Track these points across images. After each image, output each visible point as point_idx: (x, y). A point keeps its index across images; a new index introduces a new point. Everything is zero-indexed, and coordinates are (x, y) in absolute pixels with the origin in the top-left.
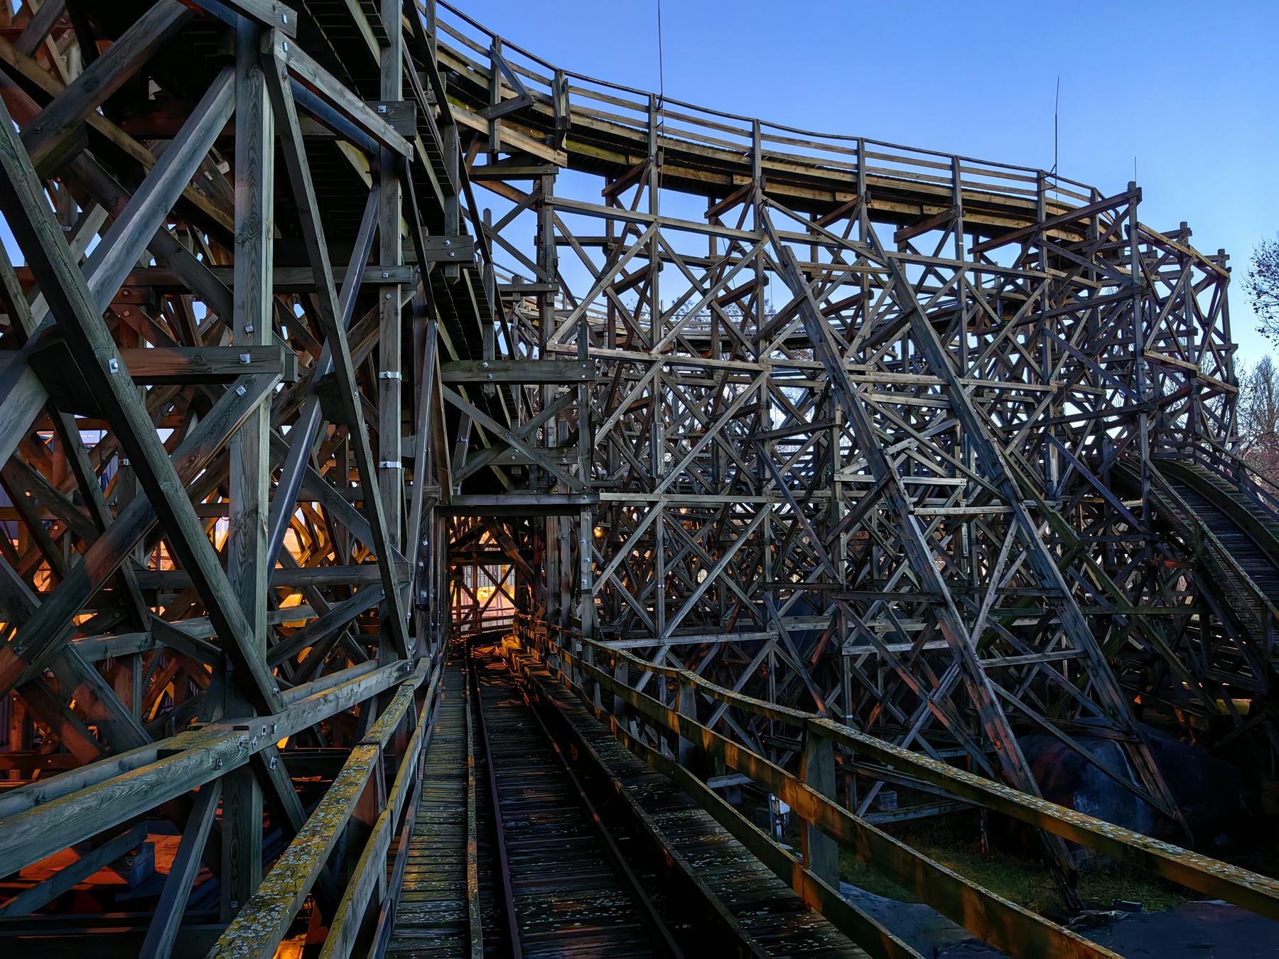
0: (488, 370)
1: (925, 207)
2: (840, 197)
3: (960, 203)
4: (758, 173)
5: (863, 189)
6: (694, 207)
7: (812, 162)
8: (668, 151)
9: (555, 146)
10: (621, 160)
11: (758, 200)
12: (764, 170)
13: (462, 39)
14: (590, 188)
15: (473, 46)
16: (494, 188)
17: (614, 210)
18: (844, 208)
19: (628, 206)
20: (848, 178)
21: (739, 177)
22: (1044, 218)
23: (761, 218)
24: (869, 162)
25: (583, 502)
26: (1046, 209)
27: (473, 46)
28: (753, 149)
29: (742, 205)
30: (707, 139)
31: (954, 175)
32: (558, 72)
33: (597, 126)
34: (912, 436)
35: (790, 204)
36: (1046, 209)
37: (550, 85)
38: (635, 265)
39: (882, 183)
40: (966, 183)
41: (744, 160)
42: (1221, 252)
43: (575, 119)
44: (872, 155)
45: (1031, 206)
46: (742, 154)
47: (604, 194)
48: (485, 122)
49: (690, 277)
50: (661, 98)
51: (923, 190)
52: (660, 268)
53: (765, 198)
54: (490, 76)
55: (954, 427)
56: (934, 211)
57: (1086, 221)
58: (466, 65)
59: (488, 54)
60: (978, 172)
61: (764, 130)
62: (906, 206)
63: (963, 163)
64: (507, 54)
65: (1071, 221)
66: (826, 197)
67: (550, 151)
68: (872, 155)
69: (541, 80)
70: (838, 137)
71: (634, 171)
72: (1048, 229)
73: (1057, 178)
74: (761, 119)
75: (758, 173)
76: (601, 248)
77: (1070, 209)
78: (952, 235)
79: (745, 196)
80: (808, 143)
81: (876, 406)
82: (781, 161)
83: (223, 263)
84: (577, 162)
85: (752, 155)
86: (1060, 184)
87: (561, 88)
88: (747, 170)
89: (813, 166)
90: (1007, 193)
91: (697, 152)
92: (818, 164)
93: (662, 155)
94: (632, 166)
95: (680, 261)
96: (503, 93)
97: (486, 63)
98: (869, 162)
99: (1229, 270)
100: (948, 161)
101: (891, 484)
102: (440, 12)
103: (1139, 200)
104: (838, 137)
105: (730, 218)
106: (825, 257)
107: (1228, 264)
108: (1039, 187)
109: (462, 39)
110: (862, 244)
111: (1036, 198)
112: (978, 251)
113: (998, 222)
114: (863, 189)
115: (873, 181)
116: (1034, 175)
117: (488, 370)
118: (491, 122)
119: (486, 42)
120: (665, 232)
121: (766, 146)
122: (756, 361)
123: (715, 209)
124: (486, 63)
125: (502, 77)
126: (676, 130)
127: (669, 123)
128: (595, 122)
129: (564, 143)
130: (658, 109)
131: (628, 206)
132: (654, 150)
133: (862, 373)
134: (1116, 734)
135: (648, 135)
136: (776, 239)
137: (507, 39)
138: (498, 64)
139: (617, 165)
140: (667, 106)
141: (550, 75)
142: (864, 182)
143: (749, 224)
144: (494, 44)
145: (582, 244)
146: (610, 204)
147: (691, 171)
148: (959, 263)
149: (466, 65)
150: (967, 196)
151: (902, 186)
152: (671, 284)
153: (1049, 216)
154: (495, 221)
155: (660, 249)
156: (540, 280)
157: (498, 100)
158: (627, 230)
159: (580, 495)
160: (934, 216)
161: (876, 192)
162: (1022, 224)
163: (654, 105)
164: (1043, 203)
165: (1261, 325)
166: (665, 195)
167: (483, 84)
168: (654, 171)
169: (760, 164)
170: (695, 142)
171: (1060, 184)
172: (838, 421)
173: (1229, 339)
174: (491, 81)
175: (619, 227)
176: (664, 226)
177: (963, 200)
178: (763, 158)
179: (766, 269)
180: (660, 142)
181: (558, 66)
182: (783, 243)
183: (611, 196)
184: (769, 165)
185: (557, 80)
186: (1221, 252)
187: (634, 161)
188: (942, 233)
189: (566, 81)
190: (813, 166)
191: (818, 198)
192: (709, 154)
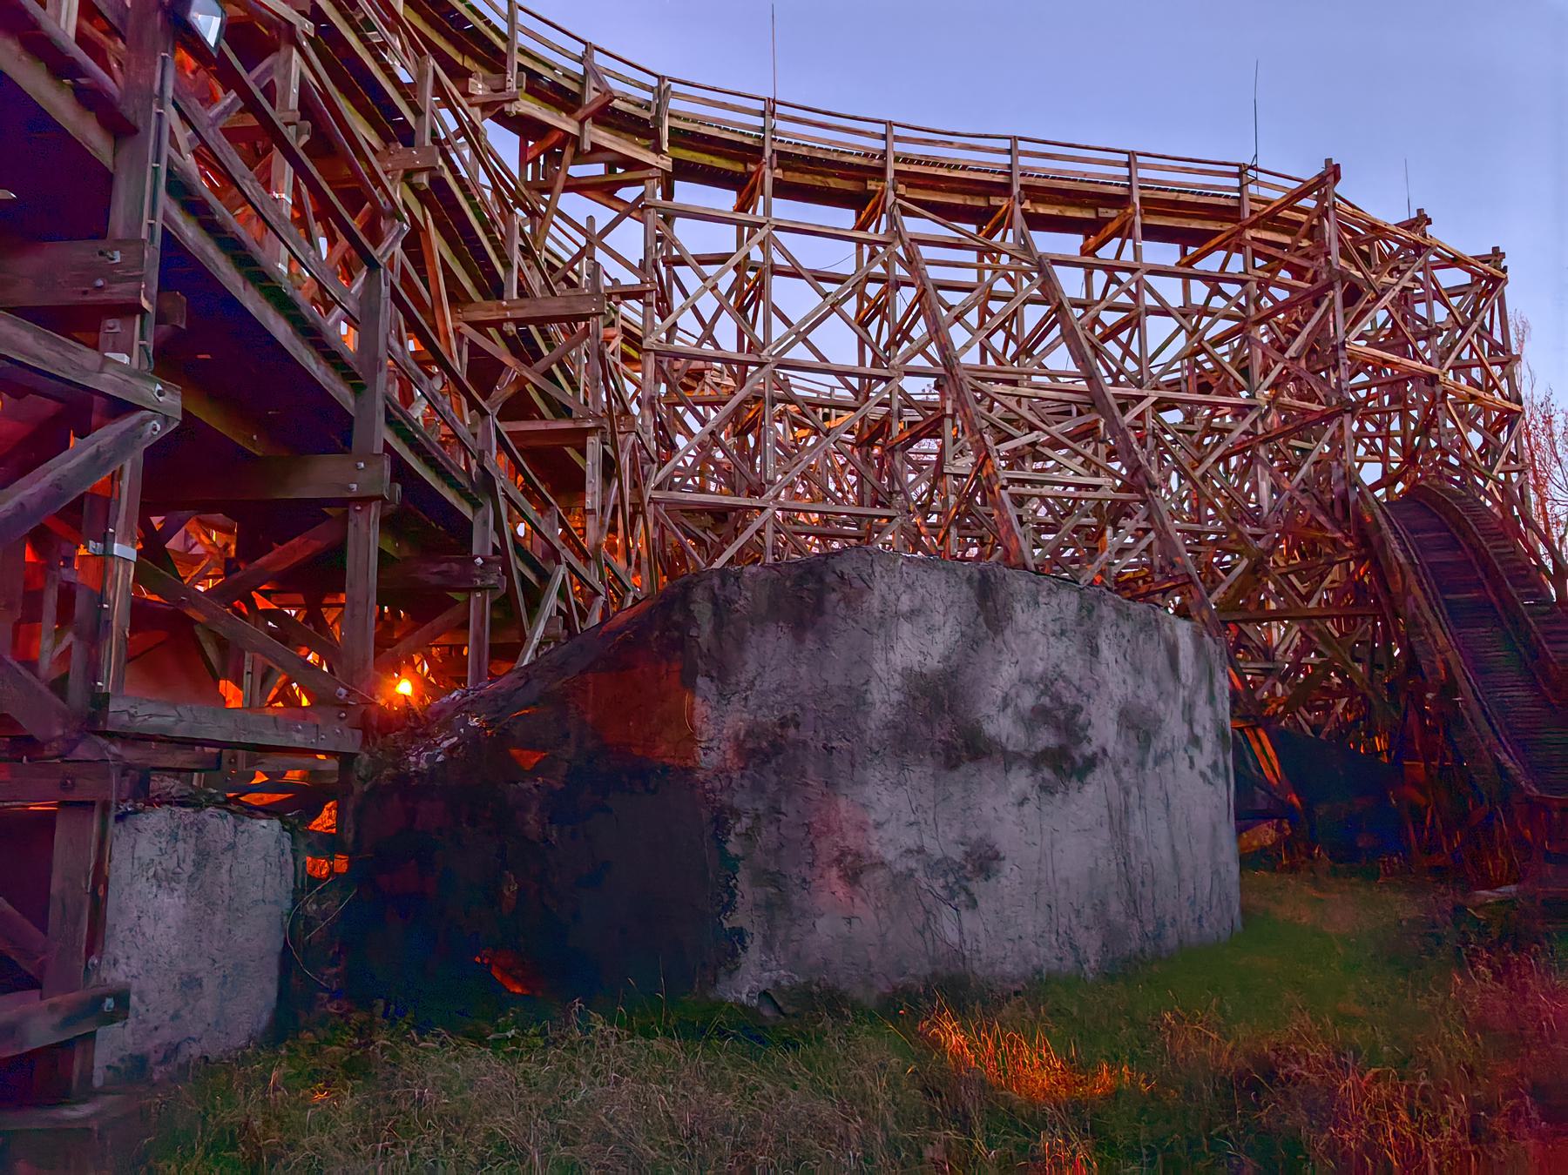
0: (506, 309)
1: (1100, 210)
3: (1136, 200)
4: (890, 175)
8: (782, 155)
10: (739, 168)
12: (897, 172)
13: (551, 46)
15: (563, 52)
16: (594, 196)
20: (1000, 179)
21: (873, 183)
22: (1247, 215)
24: (1023, 161)
26: (1248, 206)
27: (563, 52)
30: (830, 143)
32: (661, 78)
33: (704, 130)
34: (1040, 429)
39: (1041, 183)
41: (876, 162)
42: (1495, 249)
45: (1231, 203)
46: (874, 156)
48: (576, 124)
49: (819, 290)
50: (774, 101)
54: (582, 81)
55: (1097, 421)
58: (553, 69)
59: (580, 60)
60: (1161, 168)
62: (1077, 209)
63: (1140, 159)
64: (599, 60)
66: (980, 202)
67: (653, 155)
69: (643, 87)
70: (986, 136)
73: (1258, 170)
74: (894, 120)
77: (1268, 202)
80: (951, 143)
81: (996, 396)
85: (884, 154)
86: (1262, 177)
87: (662, 94)
88: (880, 173)
90: (1202, 191)
91: (819, 156)
96: (591, 96)
97: (579, 69)
98: (1023, 161)
99: (1505, 270)
100: (1125, 158)
102: (522, 18)
103: (1337, 178)
104: (986, 136)
108: (1241, 182)
109: (551, 46)
110: (1016, 247)
113: (1195, 225)
114: (1016, 190)
116: (1236, 170)
117: (506, 309)
118: (582, 123)
119: (579, 49)
121: (899, 147)
124: (579, 69)
125: (592, 83)
126: (795, 134)
127: (781, 126)
128: (702, 127)
130: (773, 114)
132: (768, 153)
137: (600, 46)
138: (591, 71)
139: (735, 173)
140: (779, 109)
141: (653, 82)
147: (819, 178)
148: (1137, 265)
149: (553, 69)
150: (1147, 194)
151: (1065, 185)
163: (770, 109)
167: (574, 88)
170: (817, 145)
171: (1262, 177)
172: (949, 411)
174: (582, 85)
176: (778, 228)
177: (1142, 199)
178: (896, 160)
180: (776, 146)
181: (660, 73)
185: (659, 87)
186: (1495, 249)
188: (1119, 240)
191: (969, 202)
192: (835, 157)
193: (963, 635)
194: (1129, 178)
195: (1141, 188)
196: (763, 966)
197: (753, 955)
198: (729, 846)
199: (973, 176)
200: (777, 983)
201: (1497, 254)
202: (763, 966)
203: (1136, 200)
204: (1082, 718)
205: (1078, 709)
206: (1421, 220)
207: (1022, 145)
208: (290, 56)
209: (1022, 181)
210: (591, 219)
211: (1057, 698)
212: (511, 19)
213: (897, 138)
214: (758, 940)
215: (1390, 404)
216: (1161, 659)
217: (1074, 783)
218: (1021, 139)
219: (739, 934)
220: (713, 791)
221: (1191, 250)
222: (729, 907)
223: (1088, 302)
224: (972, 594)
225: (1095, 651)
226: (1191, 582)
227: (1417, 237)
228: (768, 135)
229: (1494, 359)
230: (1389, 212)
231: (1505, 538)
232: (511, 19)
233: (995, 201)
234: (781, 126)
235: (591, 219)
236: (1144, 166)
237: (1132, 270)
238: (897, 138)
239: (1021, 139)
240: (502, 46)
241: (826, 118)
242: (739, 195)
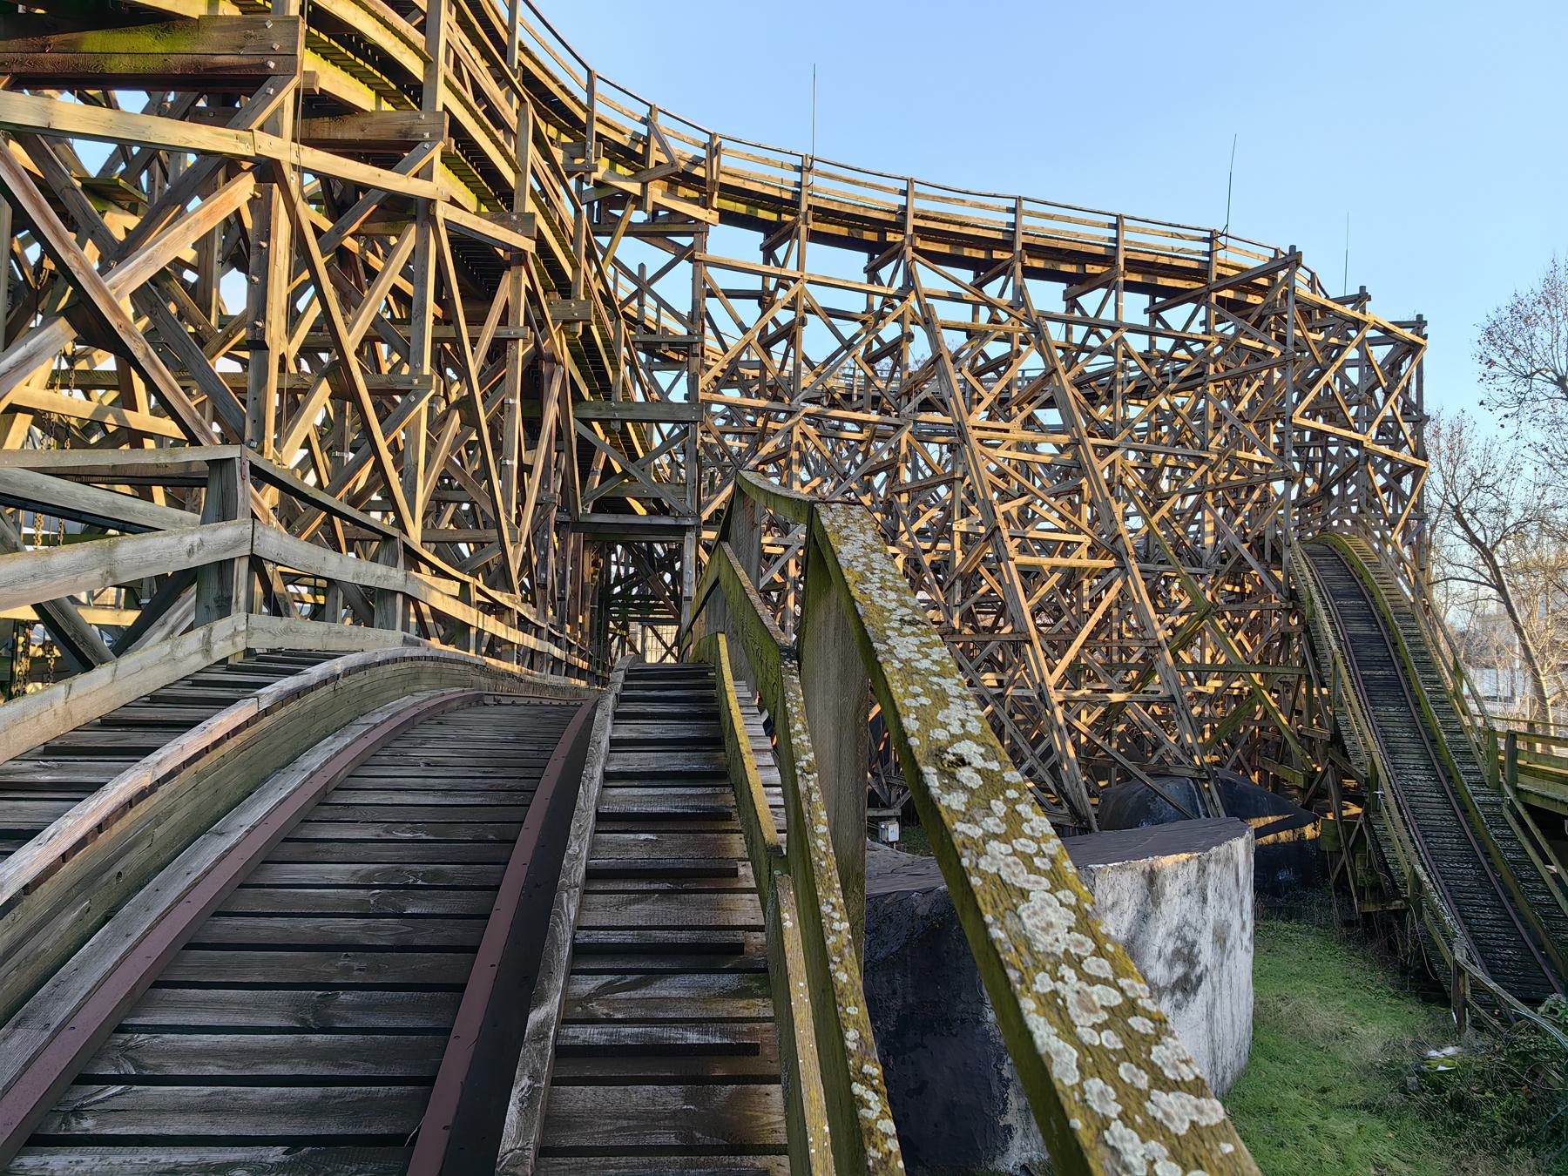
0: (615, 410)
2: (997, 255)
3: (1121, 262)
5: (1019, 247)
6: (853, 263)
7: (966, 221)
8: (816, 209)
9: (705, 203)
10: (773, 217)
11: (908, 258)
12: (916, 228)
14: (742, 245)
17: (875, 288)
18: (1001, 266)
19: (886, 281)
22: (1214, 279)
23: (910, 276)
25: (687, 523)
26: (1217, 269)
28: (905, 208)
29: (1003, 278)
31: (1118, 234)
32: (713, 136)
35: (935, 258)
36: (1217, 269)
37: (704, 147)
38: (785, 317)
39: (1039, 242)
40: (1130, 242)
43: (724, 179)
44: (1030, 214)
47: (866, 270)
50: (812, 158)
51: (1084, 248)
52: (803, 322)
53: (915, 255)
56: (1098, 269)
57: (1263, 281)
59: (644, 121)
61: (918, 188)
63: (1126, 222)
64: (662, 121)
65: (1245, 281)
68: (1030, 214)
71: (785, 229)
72: (1216, 290)
75: (910, 231)
76: (756, 302)
78: (1203, 308)
79: (1005, 269)
80: (963, 201)
82: (935, 220)
83: (271, 565)
84: (727, 217)
86: (1231, 242)
87: (714, 150)
88: (899, 226)
89: (967, 225)
91: (848, 211)
92: (972, 222)
93: (811, 213)
94: (786, 223)
95: (823, 314)
96: (656, 156)
97: (643, 130)
99: (1425, 337)
101: (997, 532)
105: (992, 290)
106: (1079, 332)
107: (1425, 331)
108: (1211, 247)
111: (1207, 259)
112: (1154, 312)
115: (1030, 240)
116: (1208, 235)
117: (615, 410)
120: (809, 287)
121: (918, 205)
122: (897, 416)
123: (979, 280)
124: (643, 130)
125: (654, 144)
126: (827, 190)
127: (819, 182)
129: (716, 202)
130: (810, 169)
131: (886, 281)
132: (804, 208)
133: (1007, 431)
134: (1191, 772)
135: (799, 194)
136: (921, 296)
142: (1021, 239)
143: (1008, 295)
144: (651, 113)
145: (728, 297)
146: (870, 282)
150: (1131, 256)
151: (1061, 245)
152: (817, 341)
153: (1220, 276)
154: (648, 276)
155: (805, 302)
156: (689, 333)
157: (652, 165)
158: (779, 285)
159: (684, 517)
160: (1098, 275)
161: (1032, 250)
162: (1195, 285)
164: (1214, 264)
165: (1484, 397)
166: (814, 250)
168: (803, 229)
169: (911, 222)
173: (1421, 411)
174: (646, 148)
175: (772, 283)
176: (810, 282)
179: (912, 323)
180: (812, 201)
182: (928, 301)
183: (768, 251)
184: (921, 223)
186: (1420, 317)
187: (786, 218)
189: (720, 144)
190: (967, 225)
193: (1138, 911)
194: (1116, 240)
195: (1126, 250)
196: (1022, 1149)
197: (1017, 1142)
198: (1003, 1072)
199: (981, 233)
200: (1031, 1160)
201: (1419, 324)
202: (1022, 1149)
203: (1121, 262)
204: (1196, 950)
205: (1194, 944)
206: (1361, 299)
207: (1026, 206)
208: (520, 274)
209: (1024, 239)
210: (642, 267)
211: (1184, 939)
212: (590, 89)
213: (917, 195)
214: (1020, 1132)
215: (1311, 439)
216: (1231, 880)
217: (1192, 997)
218: (1025, 199)
219: (1009, 1128)
220: (994, 1036)
221: (1158, 300)
222: (1004, 1112)
223: (1066, 345)
224: (1145, 882)
225: (1205, 900)
226: (1159, 646)
227: (1357, 314)
228: (804, 190)
229: (1407, 417)
230: (1336, 286)
231: (1414, 619)
232: (590, 89)
233: (997, 255)
234: (819, 182)
235: (642, 267)
236: (1130, 230)
237: (1114, 329)
238: (917, 195)
239: (1025, 199)
240: (583, 116)
241: (854, 174)
242: (767, 237)
